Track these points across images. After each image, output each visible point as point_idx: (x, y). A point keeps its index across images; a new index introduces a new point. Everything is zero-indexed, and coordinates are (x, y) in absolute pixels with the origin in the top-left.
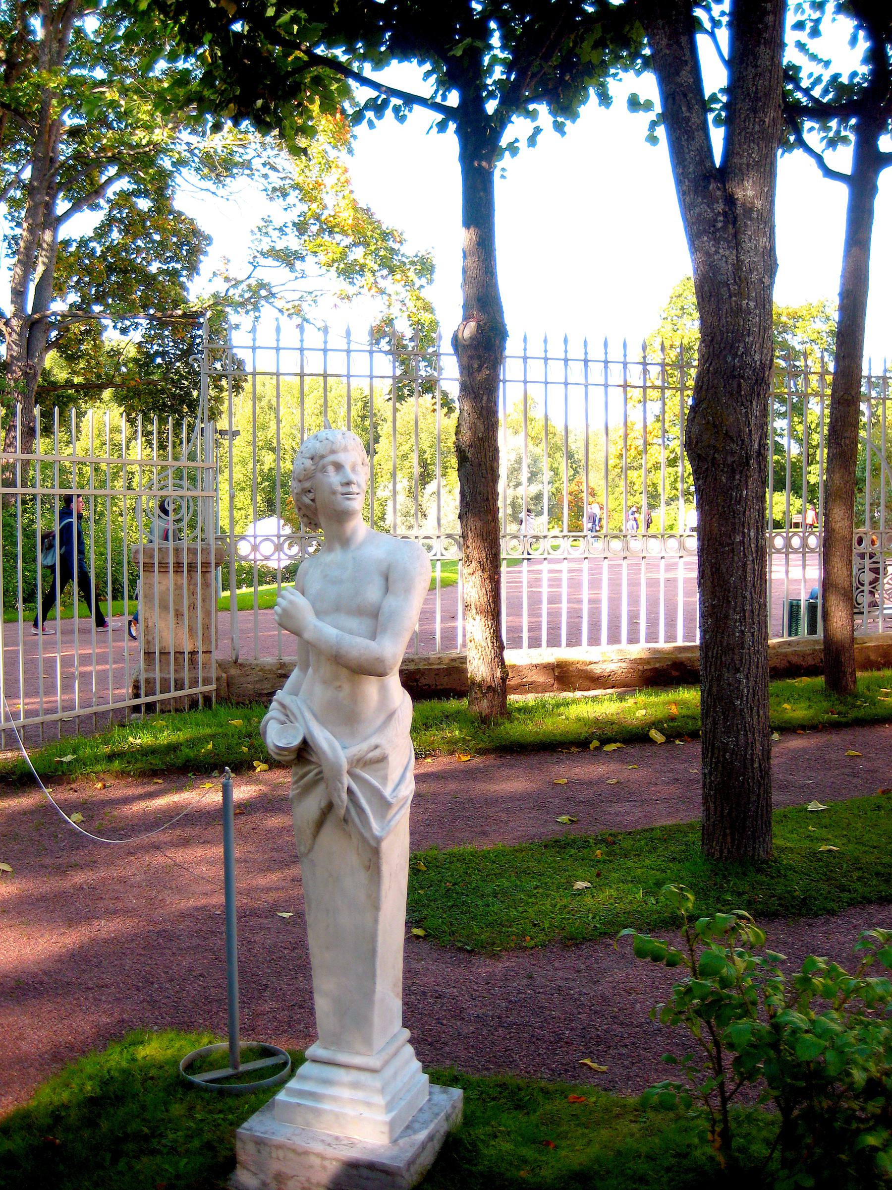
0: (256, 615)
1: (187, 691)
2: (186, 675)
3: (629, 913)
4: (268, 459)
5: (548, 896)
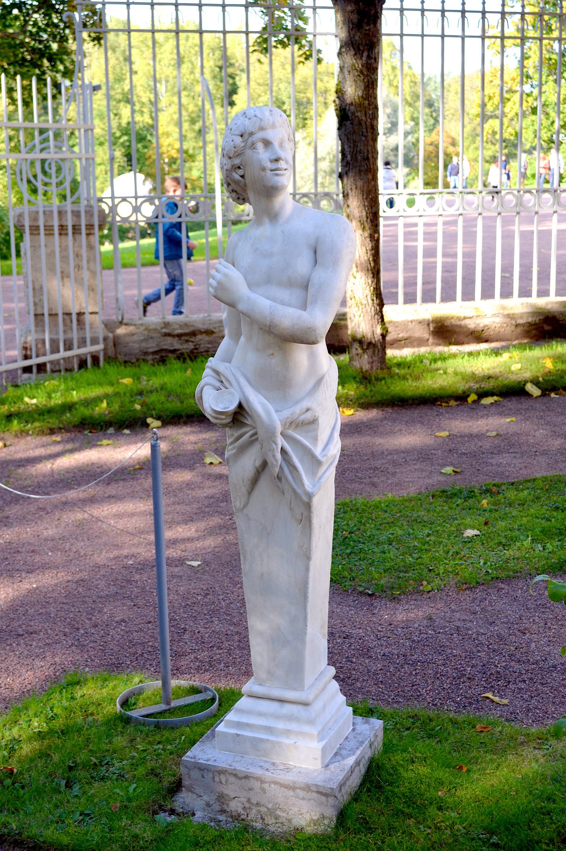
0: (139, 273)
1: (76, 352)
2: (75, 335)
3: (518, 559)
4: (125, 111)
5: (440, 543)
